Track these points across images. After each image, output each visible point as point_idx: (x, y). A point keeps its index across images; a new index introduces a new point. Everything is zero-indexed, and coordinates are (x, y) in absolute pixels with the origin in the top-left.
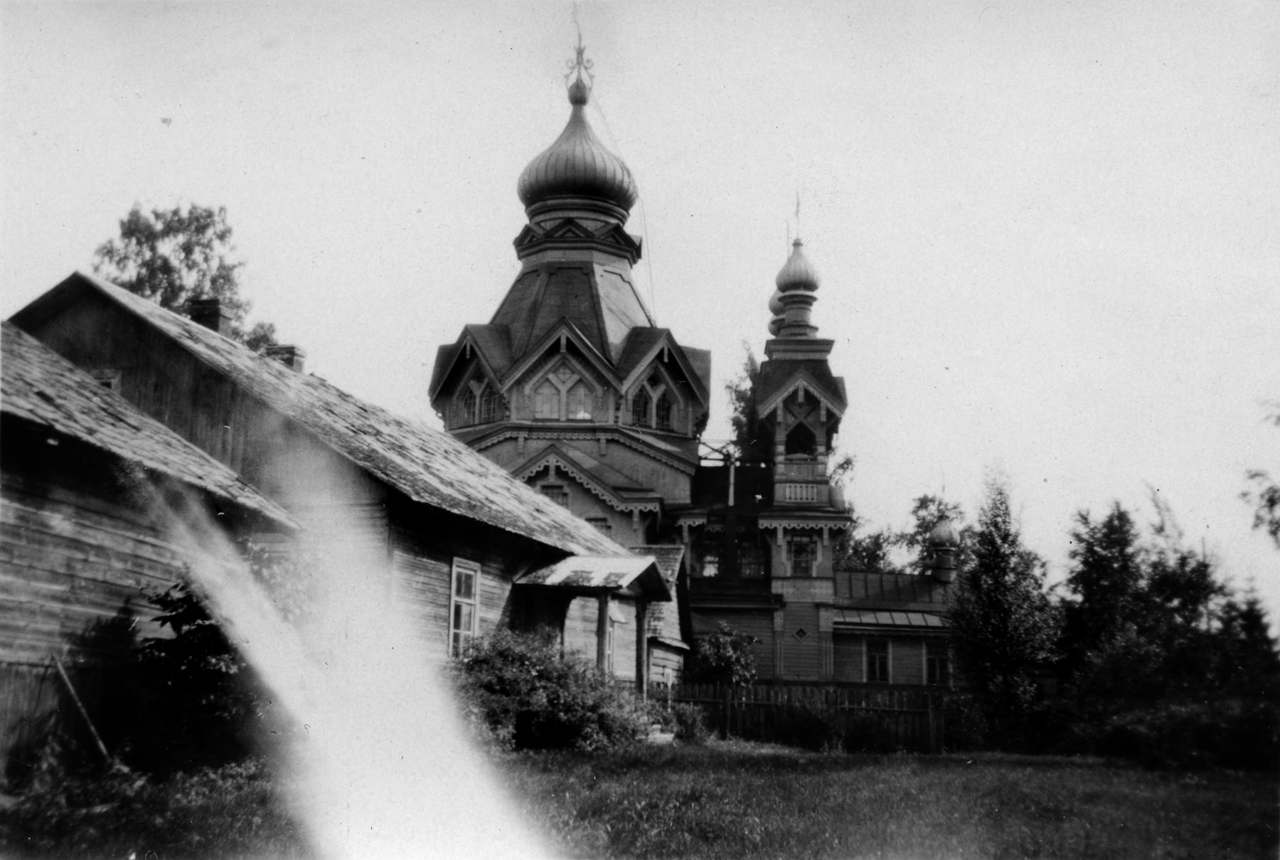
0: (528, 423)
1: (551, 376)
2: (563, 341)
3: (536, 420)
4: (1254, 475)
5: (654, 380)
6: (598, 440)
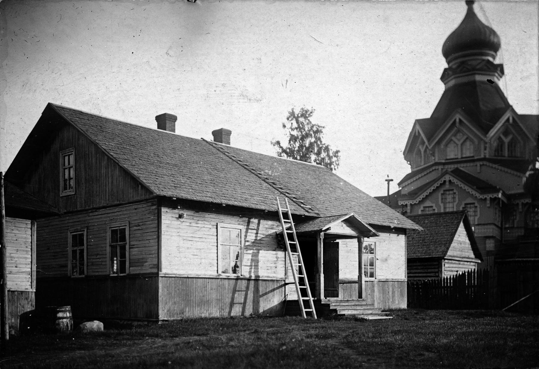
0: (443, 161)
1: (453, 138)
2: (458, 120)
3: (447, 160)
4: (284, 126)
5: (506, 133)
6: (476, 165)
